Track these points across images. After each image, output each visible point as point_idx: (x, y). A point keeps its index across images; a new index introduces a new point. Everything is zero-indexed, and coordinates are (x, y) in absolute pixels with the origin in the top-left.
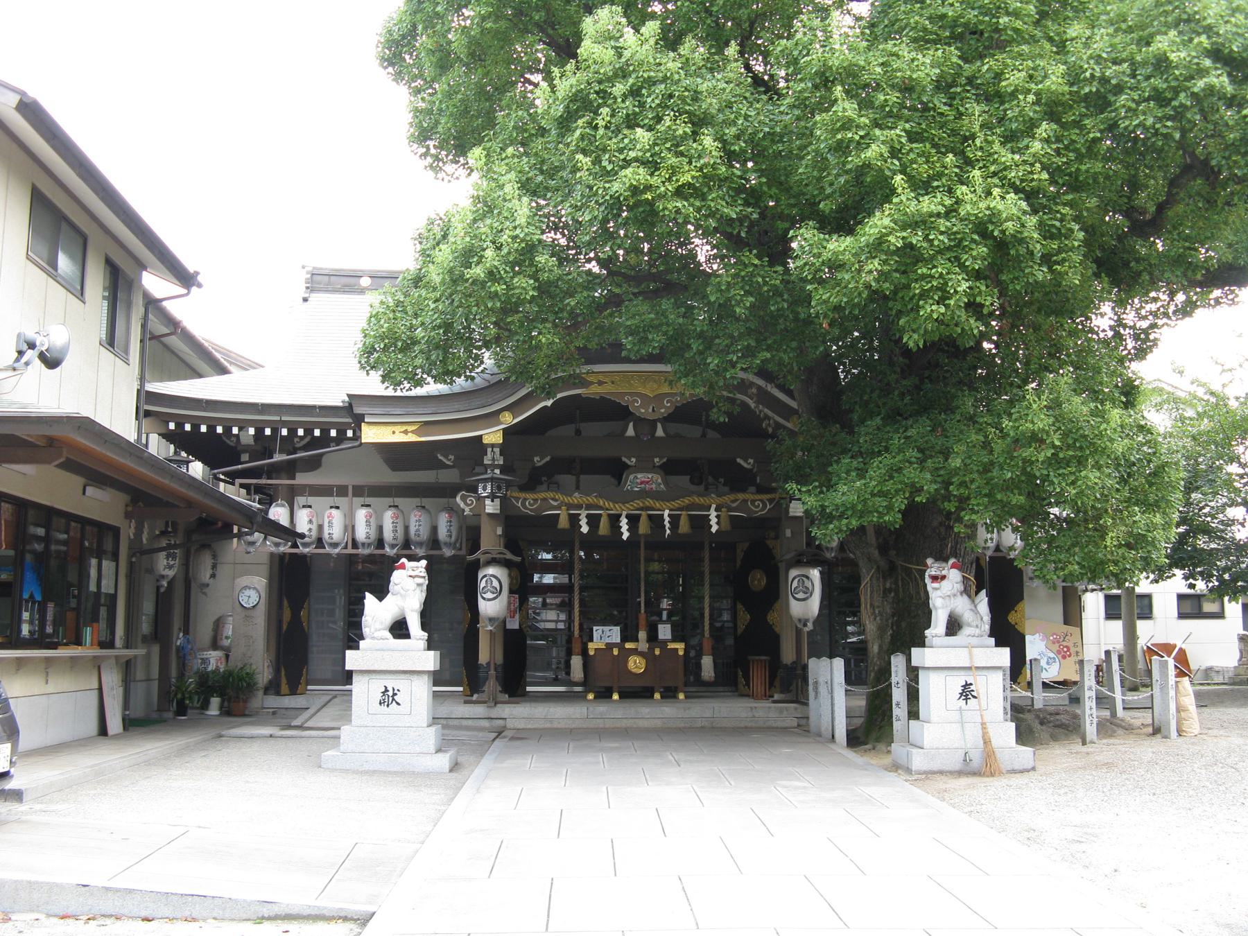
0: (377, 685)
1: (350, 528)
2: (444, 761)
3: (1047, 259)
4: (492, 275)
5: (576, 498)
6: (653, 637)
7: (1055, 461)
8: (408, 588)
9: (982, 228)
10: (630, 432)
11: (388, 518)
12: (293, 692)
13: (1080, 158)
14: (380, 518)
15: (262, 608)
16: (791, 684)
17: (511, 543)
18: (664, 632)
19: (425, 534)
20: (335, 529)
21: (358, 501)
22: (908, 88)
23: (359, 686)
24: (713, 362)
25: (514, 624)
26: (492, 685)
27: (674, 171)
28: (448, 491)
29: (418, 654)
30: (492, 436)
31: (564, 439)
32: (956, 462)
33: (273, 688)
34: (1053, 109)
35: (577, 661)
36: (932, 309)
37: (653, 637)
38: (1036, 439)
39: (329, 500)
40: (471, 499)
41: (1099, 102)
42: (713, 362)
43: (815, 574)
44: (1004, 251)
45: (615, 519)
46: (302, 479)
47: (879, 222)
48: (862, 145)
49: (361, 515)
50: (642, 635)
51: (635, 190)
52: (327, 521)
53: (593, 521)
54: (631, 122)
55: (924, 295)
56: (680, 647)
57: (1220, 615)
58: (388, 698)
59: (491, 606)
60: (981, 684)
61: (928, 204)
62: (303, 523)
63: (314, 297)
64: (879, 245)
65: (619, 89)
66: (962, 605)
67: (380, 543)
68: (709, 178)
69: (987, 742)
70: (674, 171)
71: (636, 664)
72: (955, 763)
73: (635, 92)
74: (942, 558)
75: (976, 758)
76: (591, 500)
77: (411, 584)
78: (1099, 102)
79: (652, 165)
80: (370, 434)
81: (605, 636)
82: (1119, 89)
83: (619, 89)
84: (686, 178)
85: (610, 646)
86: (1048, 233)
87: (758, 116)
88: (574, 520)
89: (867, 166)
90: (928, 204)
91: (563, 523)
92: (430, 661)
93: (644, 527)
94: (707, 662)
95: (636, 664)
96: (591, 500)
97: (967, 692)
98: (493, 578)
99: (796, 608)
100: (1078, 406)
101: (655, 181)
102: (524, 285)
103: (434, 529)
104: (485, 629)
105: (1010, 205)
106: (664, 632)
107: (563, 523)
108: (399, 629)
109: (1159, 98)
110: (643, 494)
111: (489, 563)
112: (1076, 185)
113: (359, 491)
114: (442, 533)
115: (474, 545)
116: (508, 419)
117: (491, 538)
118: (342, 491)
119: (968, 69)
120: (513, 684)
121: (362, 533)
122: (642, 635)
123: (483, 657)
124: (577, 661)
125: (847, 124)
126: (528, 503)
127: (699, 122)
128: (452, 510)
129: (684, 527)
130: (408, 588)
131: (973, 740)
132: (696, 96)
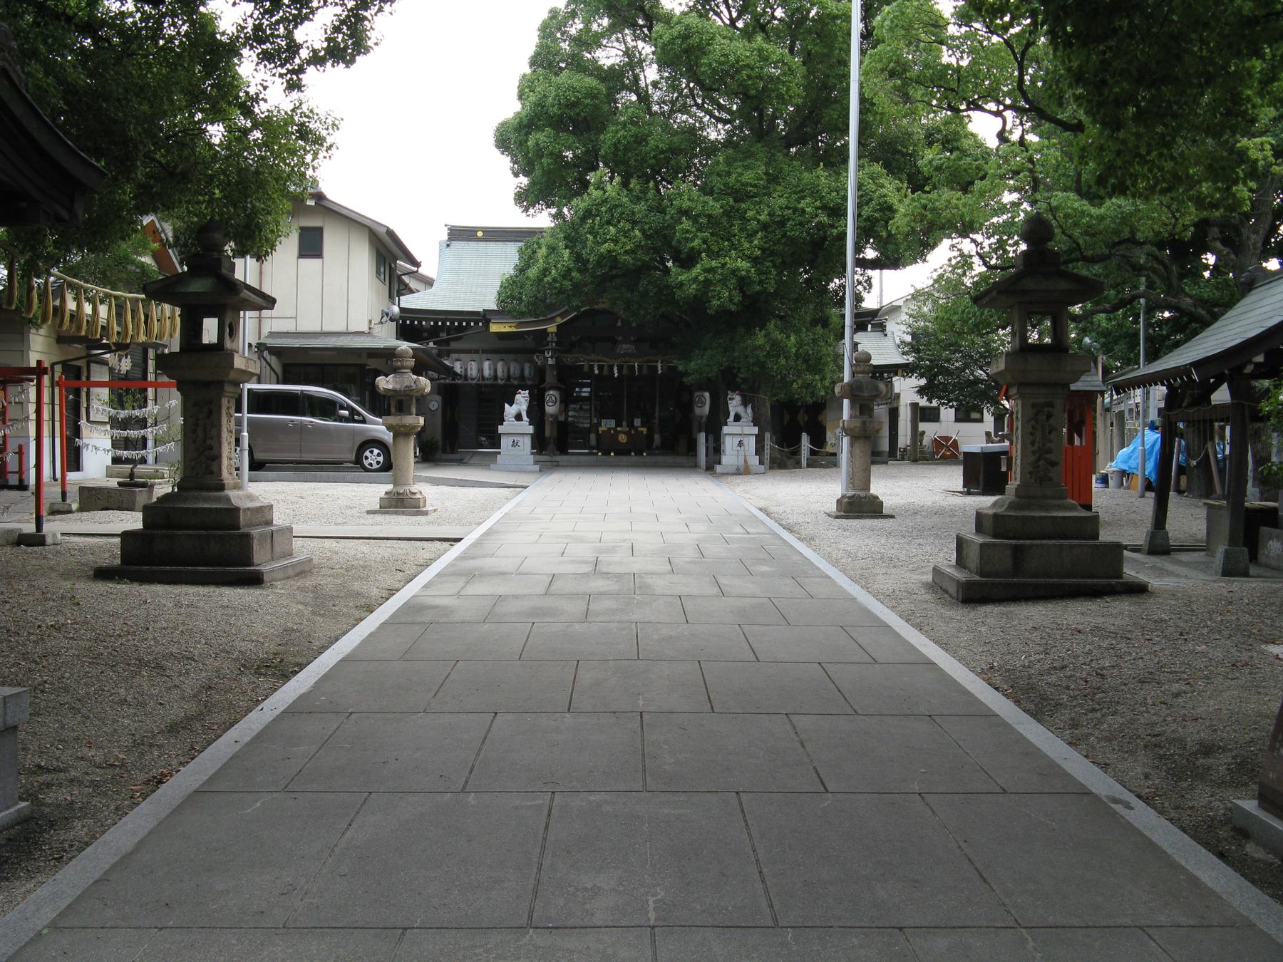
0: (510, 440)
1: (481, 370)
2: (537, 467)
3: (761, 282)
4: (555, 280)
5: (593, 357)
6: (631, 425)
7: (768, 356)
8: (522, 400)
9: (734, 272)
10: (619, 324)
11: (500, 366)
12: (452, 452)
13: (774, 244)
14: (495, 365)
15: (179, 408)
16: (692, 449)
17: (561, 378)
18: (637, 422)
19: (518, 373)
20: (473, 371)
21: (485, 356)
22: (710, 216)
23: (504, 441)
24: (642, 312)
25: (562, 418)
26: (552, 447)
27: (624, 244)
28: (533, 352)
29: (527, 427)
30: (552, 328)
31: (586, 331)
32: (736, 355)
33: (444, 451)
34: (764, 227)
35: (593, 436)
36: (715, 303)
37: (631, 425)
38: (760, 348)
39: (470, 356)
40: (541, 357)
41: (782, 223)
42: (642, 312)
43: (707, 395)
44: (743, 282)
45: (611, 368)
46: (454, 345)
47: (697, 270)
48: (692, 240)
49: (486, 364)
50: (624, 423)
51: (609, 252)
52: (473, 367)
53: (600, 368)
54: (608, 223)
55: (713, 297)
56: (644, 430)
57: (981, 420)
58: (515, 444)
59: (551, 409)
60: (746, 440)
61: (714, 264)
62: (458, 368)
63: (455, 244)
64: (695, 280)
65: (603, 209)
66: (741, 410)
67: (496, 377)
68: (639, 246)
69: (746, 462)
70: (624, 244)
71: (622, 438)
72: (733, 470)
73: (610, 209)
74: (733, 391)
75: (742, 469)
76: (599, 357)
77: (523, 400)
78: (782, 223)
79: (616, 241)
80: (494, 328)
81: (607, 424)
82: (789, 220)
83: (603, 209)
84: (628, 248)
85: (609, 429)
86: (760, 272)
87: (656, 218)
88: (591, 367)
89: (693, 248)
90: (714, 264)
91: (586, 369)
92: (531, 430)
93: (625, 372)
94: (657, 437)
95: (622, 438)
96: (599, 357)
97: (740, 444)
98: (552, 395)
99: (698, 411)
100: (778, 335)
101: (617, 248)
102: (567, 284)
103: (522, 370)
104: (548, 420)
105: (743, 265)
106: (637, 422)
107: (586, 369)
108: (518, 417)
109: (801, 224)
110: (625, 355)
111: (551, 388)
112: (772, 253)
113: (484, 352)
114: (527, 373)
115: (543, 380)
116: (559, 321)
117: (550, 377)
118: (476, 352)
119: (737, 206)
120: (562, 448)
121: (487, 373)
122: (624, 423)
123: (547, 433)
124: (593, 436)
125: (688, 232)
126: (568, 359)
127: (634, 223)
128: (531, 361)
129: (645, 371)
130: (522, 400)
131: (741, 462)
132: (633, 213)
